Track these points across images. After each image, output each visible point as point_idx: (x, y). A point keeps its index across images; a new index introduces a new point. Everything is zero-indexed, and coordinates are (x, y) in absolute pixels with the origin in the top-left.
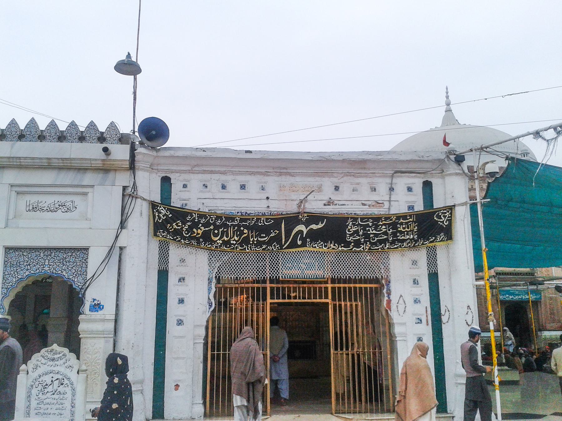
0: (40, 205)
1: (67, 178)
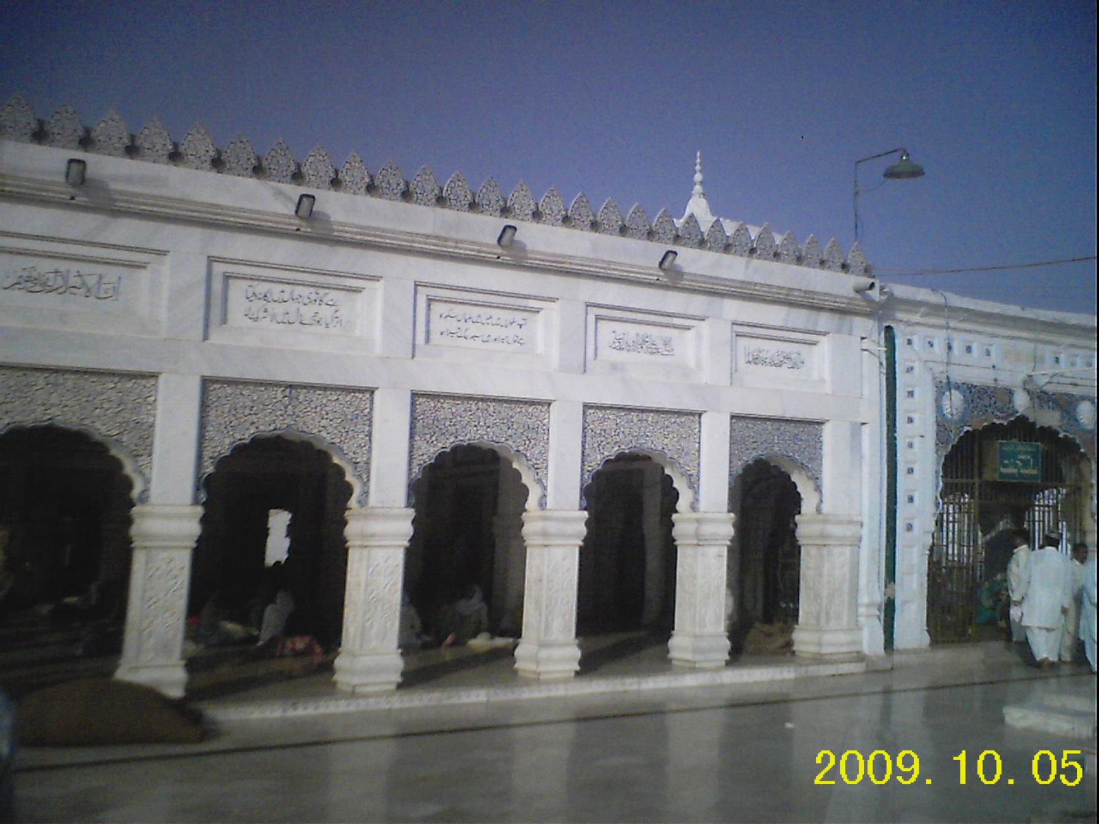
0: (761, 355)
1: (799, 317)
